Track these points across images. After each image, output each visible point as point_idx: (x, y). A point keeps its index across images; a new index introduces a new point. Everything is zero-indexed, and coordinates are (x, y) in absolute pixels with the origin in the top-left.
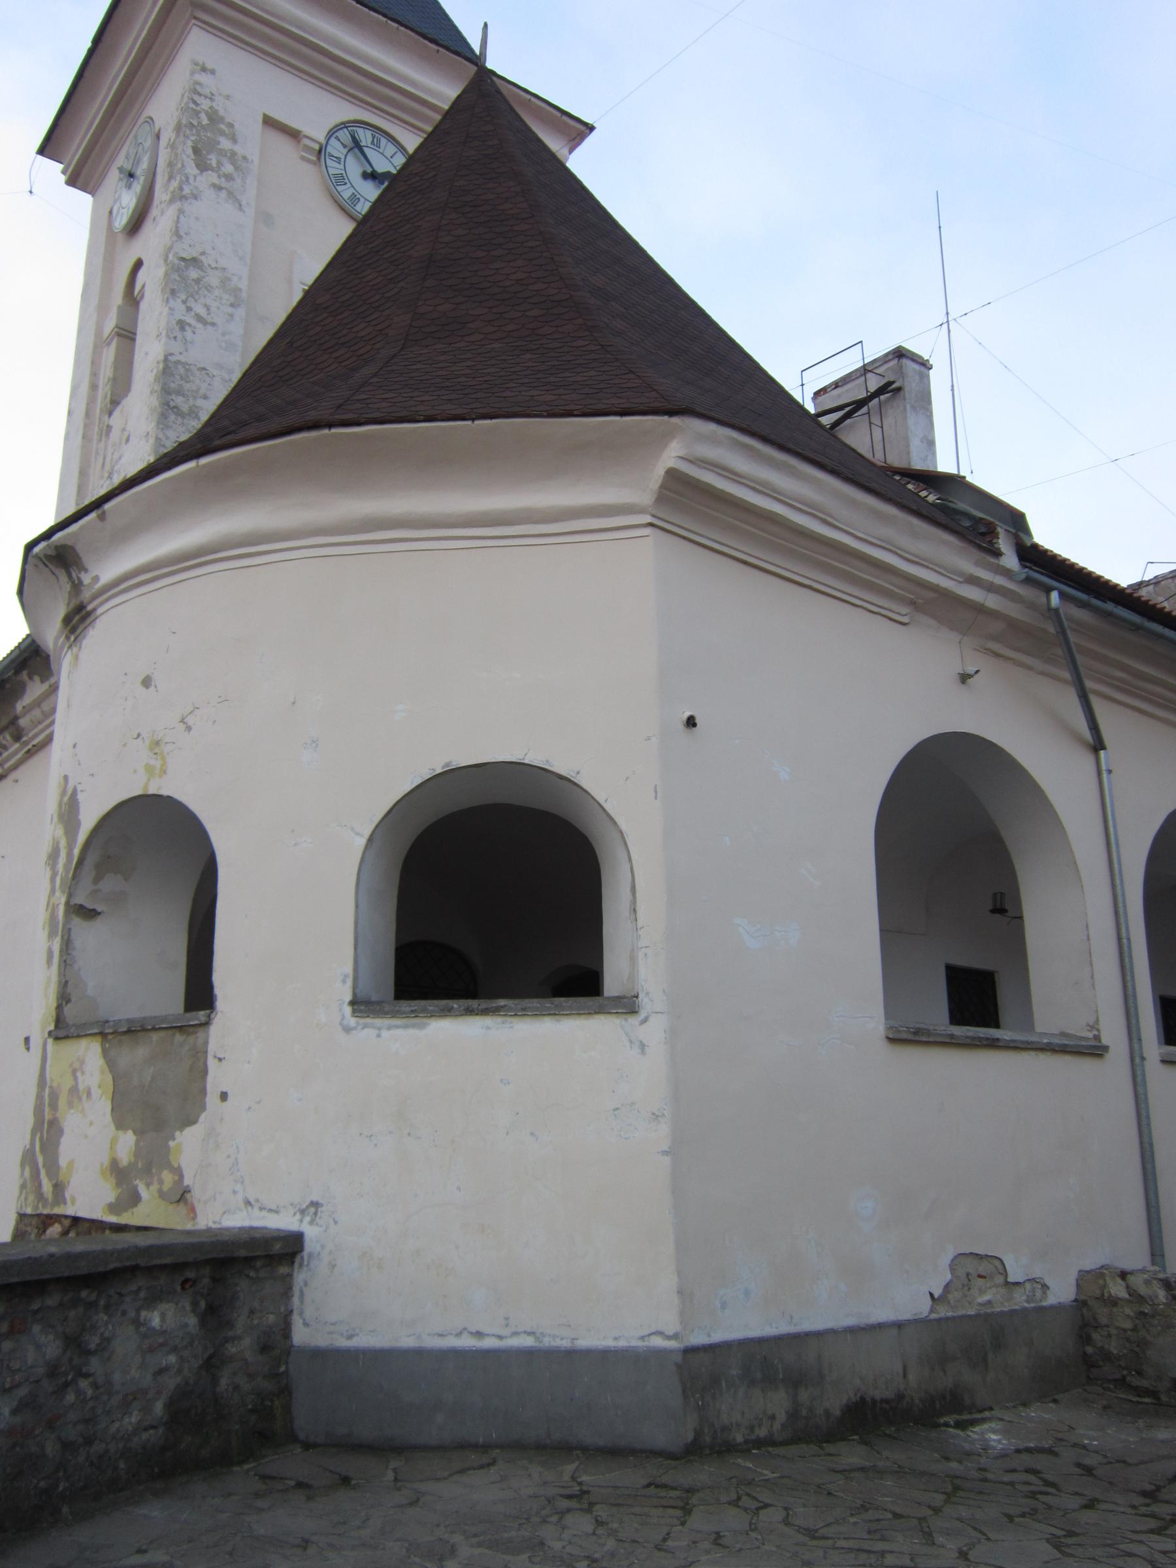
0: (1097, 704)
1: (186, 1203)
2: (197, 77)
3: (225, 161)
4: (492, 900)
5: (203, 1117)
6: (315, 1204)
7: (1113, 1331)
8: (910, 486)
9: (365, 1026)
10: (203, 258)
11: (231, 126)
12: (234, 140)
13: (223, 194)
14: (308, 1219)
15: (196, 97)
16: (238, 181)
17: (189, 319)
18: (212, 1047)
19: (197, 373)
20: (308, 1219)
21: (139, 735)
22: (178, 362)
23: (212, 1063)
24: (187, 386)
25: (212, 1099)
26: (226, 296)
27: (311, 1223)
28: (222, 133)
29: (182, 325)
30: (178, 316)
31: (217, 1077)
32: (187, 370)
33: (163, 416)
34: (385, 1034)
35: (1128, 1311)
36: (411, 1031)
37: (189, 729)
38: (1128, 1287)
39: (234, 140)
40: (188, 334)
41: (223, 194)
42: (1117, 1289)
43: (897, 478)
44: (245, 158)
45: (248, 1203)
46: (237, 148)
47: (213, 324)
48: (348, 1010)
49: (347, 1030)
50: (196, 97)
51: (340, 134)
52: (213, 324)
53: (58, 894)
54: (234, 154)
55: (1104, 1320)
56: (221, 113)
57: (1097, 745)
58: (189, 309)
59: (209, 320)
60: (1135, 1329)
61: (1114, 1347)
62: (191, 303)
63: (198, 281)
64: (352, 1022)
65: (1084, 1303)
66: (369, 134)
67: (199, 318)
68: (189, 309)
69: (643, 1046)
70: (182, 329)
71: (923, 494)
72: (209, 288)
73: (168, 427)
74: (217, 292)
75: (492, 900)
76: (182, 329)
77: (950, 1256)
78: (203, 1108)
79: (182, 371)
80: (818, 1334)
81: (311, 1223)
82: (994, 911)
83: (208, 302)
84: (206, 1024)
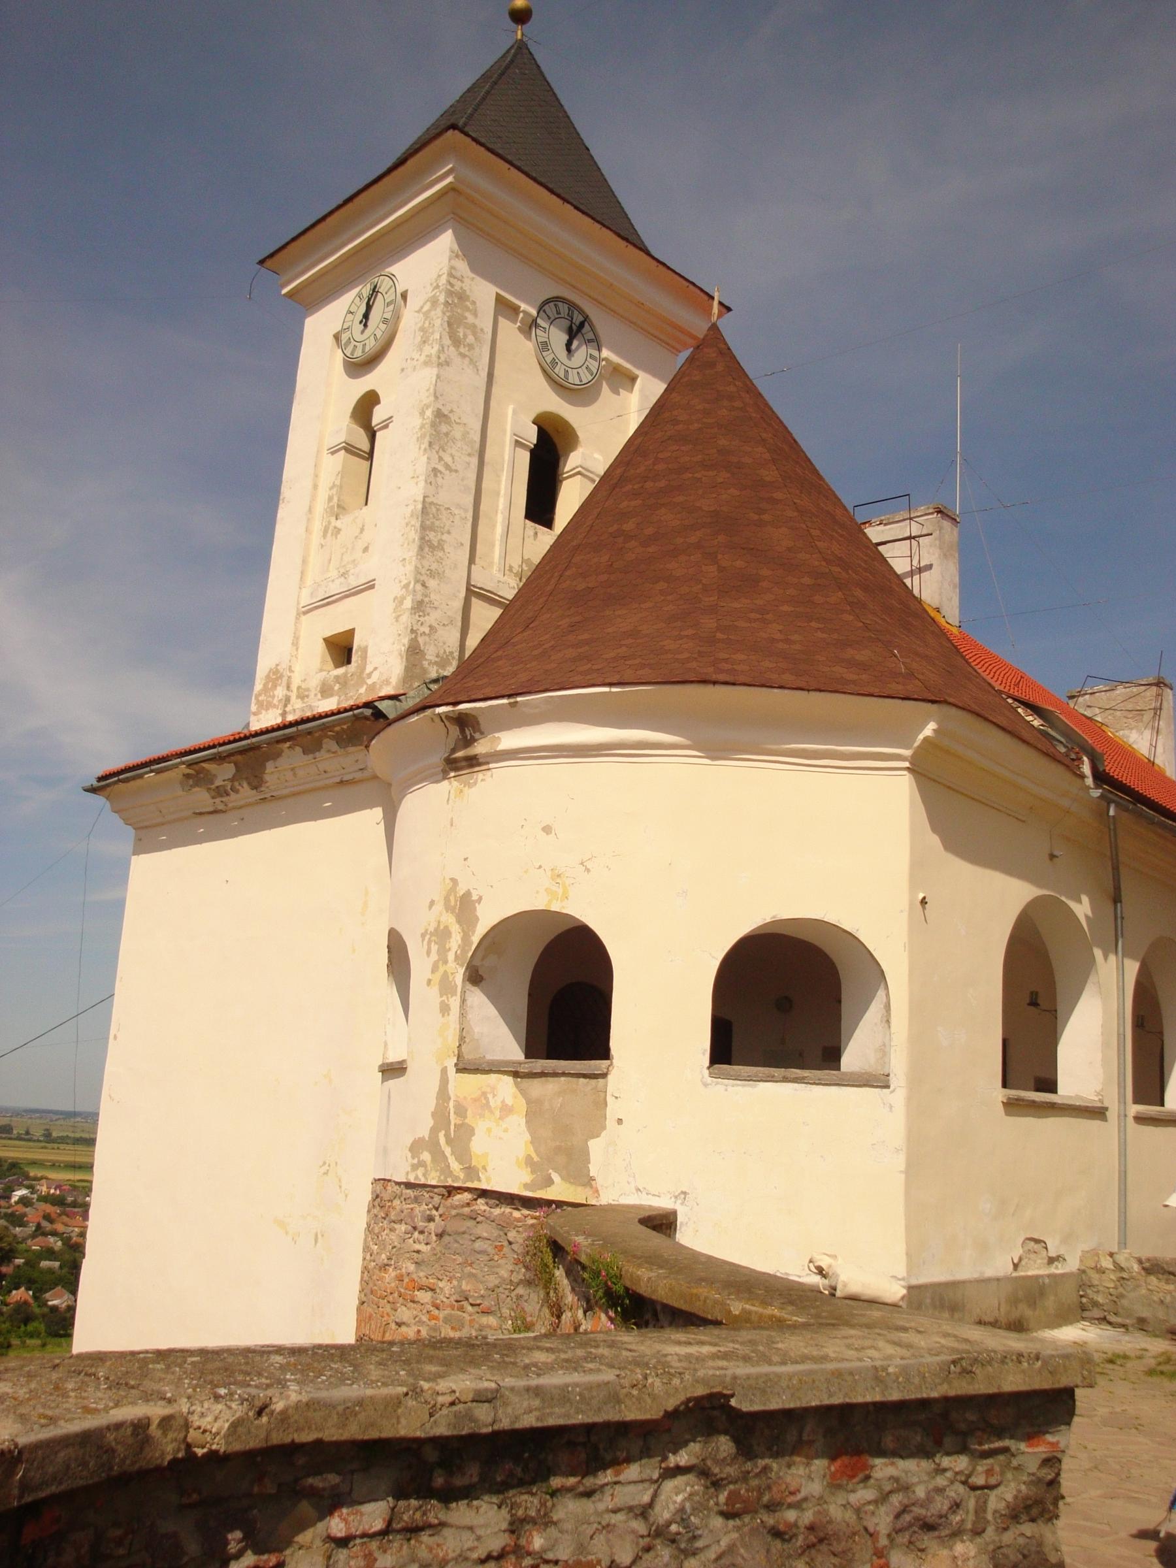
0: (1123, 871)
1: (591, 1187)
2: (453, 262)
3: (469, 332)
4: (783, 1002)
5: (603, 1134)
6: (685, 1193)
7: (1101, 1289)
8: (1020, 710)
9: (717, 1083)
10: (451, 415)
11: (474, 303)
12: (475, 315)
13: (467, 361)
14: (679, 1201)
15: (452, 280)
16: (477, 349)
17: (441, 467)
18: (610, 1090)
19: (444, 512)
20: (679, 1201)
21: (540, 867)
22: (432, 503)
23: (609, 1099)
24: (437, 523)
25: (610, 1122)
26: (465, 447)
27: (682, 1204)
28: (468, 309)
29: (435, 471)
30: (433, 465)
31: (613, 1109)
32: (438, 510)
33: (421, 548)
34: (730, 1089)
35: (1112, 1277)
36: (747, 1089)
37: (588, 870)
38: (1114, 1262)
39: (475, 315)
40: (439, 480)
41: (467, 361)
42: (1107, 1263)
43: (1010, 701)
44: (482, 330)
45: (638, 1190)
46: (477, 322)
47: (456, 471)
48: (706, 1072)
49: (706, 1085)
50: (452, 280)
51: (546, 307)
52: (456, 471)
53: (452, 964)
54: (474, 326)
55: (1096, 1282)
56: (468, 293)
57: (1117, 899)
58: (441, 459)
59: (454, 468)
60: (1116, 1288)
61: (1100, 1299)
62: (441, 453)
63: (447, 434)
64: (709, 1080)
65: (1084, 1272)
66: (566, 306)
67: (447, 467)
68: (441, 459)
69: (891, 1107)
70: (436, 475)
71: (1029, 718)
72: (454, 440)
73: (423, 557)
74: (459, 444)
75: (783, 1002)
76: (436, 475)
77: (1022, 1239)
78: (604, 1128)
79: (434, 510)
80: (964, 1282)
81: (682, 1204)
82: (1030, 1004)
83: (454, 452)
84: (604, 1076)
